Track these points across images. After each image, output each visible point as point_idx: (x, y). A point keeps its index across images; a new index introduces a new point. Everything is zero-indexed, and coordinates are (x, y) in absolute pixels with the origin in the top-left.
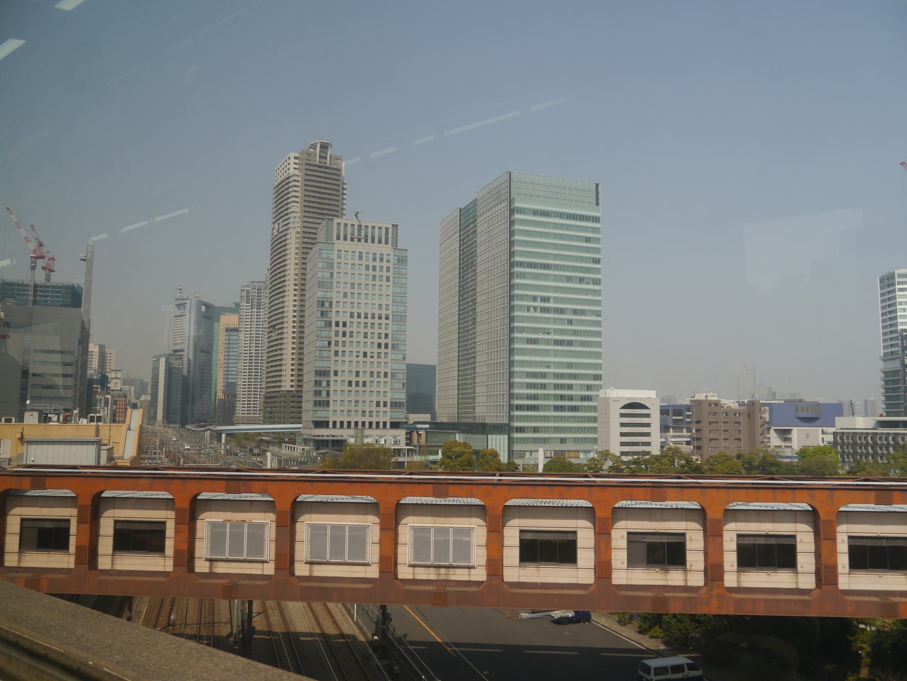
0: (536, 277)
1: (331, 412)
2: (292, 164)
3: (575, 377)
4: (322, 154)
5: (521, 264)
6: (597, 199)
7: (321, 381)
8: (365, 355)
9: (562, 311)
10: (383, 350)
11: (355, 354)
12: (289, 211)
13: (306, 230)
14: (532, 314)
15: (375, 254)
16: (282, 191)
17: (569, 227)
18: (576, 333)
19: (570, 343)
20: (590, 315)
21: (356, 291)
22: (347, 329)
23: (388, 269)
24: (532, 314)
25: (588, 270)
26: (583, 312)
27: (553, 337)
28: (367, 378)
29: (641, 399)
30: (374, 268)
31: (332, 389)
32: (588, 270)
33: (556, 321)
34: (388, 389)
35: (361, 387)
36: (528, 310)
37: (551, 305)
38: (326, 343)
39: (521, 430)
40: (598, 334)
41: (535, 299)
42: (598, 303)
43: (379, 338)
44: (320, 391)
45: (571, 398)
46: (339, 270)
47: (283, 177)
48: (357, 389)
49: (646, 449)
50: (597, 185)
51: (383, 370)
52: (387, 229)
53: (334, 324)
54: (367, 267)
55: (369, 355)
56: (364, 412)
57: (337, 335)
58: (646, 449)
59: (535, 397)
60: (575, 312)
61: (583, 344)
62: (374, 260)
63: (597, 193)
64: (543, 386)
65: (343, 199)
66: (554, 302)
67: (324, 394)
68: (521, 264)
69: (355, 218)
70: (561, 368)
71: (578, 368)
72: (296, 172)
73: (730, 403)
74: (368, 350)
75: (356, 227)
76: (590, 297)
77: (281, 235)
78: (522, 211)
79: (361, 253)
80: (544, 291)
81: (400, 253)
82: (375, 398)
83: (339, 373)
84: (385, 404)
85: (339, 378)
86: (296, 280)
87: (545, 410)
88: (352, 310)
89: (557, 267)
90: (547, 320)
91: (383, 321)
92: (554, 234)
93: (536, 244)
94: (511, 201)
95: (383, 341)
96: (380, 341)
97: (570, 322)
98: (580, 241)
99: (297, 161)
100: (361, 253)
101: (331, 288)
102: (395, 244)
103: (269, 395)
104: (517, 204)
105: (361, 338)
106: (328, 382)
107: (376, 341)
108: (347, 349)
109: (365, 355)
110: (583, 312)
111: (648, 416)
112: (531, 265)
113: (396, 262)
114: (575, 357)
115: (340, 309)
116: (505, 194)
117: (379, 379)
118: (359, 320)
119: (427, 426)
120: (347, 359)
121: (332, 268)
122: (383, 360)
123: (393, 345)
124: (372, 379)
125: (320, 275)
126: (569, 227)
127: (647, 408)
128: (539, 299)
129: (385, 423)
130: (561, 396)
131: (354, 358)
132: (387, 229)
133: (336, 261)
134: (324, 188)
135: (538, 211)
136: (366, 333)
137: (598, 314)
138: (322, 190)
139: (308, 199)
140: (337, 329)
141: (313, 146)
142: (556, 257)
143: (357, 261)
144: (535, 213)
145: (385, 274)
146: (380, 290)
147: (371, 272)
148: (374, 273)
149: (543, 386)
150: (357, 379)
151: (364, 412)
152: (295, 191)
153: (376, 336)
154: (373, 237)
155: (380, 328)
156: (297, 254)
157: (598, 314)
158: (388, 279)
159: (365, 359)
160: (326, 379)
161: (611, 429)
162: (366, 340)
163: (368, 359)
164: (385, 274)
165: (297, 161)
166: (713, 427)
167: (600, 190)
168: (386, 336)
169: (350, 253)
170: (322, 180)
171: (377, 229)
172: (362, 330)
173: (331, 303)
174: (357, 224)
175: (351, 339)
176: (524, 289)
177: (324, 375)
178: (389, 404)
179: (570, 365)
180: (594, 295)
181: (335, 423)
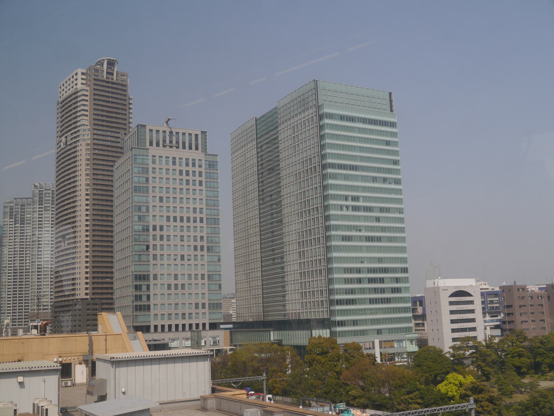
0: (346, 177)
1: (152, 316)
2: (79, 79)
3: (385, 270)
4: (109, 71)
5: (333, 166)
6: (391, 106)
7: (141, 285)
8: (182, 257)
9: (370, 209)
10: (199, 253)
11: (173, 257)
12: (78, 124)
13: (96, 142)
14: (345, 212)
15: (187, 159)
16: (68, 107)
17: (371, 131)
18: (383, 229)
19: (379, 239)
20: (395, 213)
21: (171, 195)
22: (165, 233)
23: (200, 174)
24: (345, 212)
25: (389, 171)
26: (388, 210)
27: (364, 234)
28: (186, 281)
29: (465, 287)
30: (187, 173)
31: (151, 293)
32: (389, 171)
33: (366, 219)
34: (206, 291)
35: (180, 291)
36: (341, 209)
37: (361, 204)
38: (145, 248)
39: (342, 323)
40: (402, 230)
41: (346, 198)
42: (399, 201)
43: (195, 240)
44: (141, 296)
45: (383, 291)
46: (154, 175)
47: (69, 93)
48: (177, 291)
49: (471, 334)
50: (390, 94)
51: (200, 272)
52: (196, 136)
53: (151, 229)
54: (181, 172)
55: (186, 258)
56: (184, 314)
57: (155, 239)
58: (471, 334)
59: (352, 291)
60: (382, 210)
61: (390, 239)
62: (187, 165)
63: (391, 101)
64: (359, 281)
65: (130, 113)
66: (363, 201)
67: (144, 298)
68: (333, 166)
69: (165, 125)
70: (373, 262)
71: (387, 262)
72: (84, 87)
73: (533, 288)
74: (185, 253)
75: (168, 133)
76: (393, 196)
77: (69, 147)
78: (331, 116)
79: (174, 158)
80: (354, 191)
81: (211, 158)
82: (193, 301)
83: (159, 277)
84: (204, 305)
85: (159, 282)
86: (87, 190)
87: (361, 304)
88: (168, 214)
89: (364, 169)
90: (358, 218)
91: (198, 224)
92: (359, 138)
93: (344, 147)
94: (319, 107)
95: (199, 244)
96: (196, 244)
97: (378, 219)
98: (382, 144)
99: (84, 77)
100: (174, 158)
101: (147, 192)
102: (205, 150)
103: (57, 304)
104: (326, 110)
105: (178, 241)
106: (148, 287)
107: (192, 243)
108: (165, 252)
109: (182, 257)
110: (388, 210)
111: (472, 302)
112: (341, 167)
113: (207, 166)
114: (384, 252)
115: (157, 213)
116: (309, 101)
117: (196, 282)
118: (175, 224)
119: (231, 326)
120: (165, 262)
121: (147, 172)
122: (199, 262)
123: (208, 247)
124: (189, 282)
125: (136, 179)
126: (371, 131)
127: (470, 295)
128: (350, 198)
129: (204, 325)
130: (375, 289)
131: (172, 262)
132: (196, 136)
133: (151, 166)
134: (112, 103)
135: (344, 116)
136: (182, 236)
137: (401, 211)
138: (110, 105)
139: (97, 112)
140: (154, 233)
141: (101, 63)
142: (362, 159)
143: (171, 167)
144: (342, 118)
145: (198, 178)
146: (194, 194)
147: (184, 177)
148: (187, 178)
149: (359, 281)
150: (176, 282)
151: (170, 314)
152: (84, 105)
153: (192, 240)
154: (184, 143)
155: (195, 231)
156: (88, 165)
157: (401, 211)
158: (201, 183)
159: (183, 262)
160: (146, 283)
161: (443, 317)
162: (182, 243)
163: (186, 262)
164: (198, 178)
165: (84, 77)
166: (523, 310)
167: (393, 98)
168: (202, 238)
169: (164, 159)
170: (110, 95)
171: (187, 135)
172: (179, 234)
173: (148, 207)
174: (168, 130)
175: (169, 243)
176: (337, 189)
177: (144, 279)
178: (207, 306)
179: (380, 260)
180: (396, 194)
181: (156, 327)
